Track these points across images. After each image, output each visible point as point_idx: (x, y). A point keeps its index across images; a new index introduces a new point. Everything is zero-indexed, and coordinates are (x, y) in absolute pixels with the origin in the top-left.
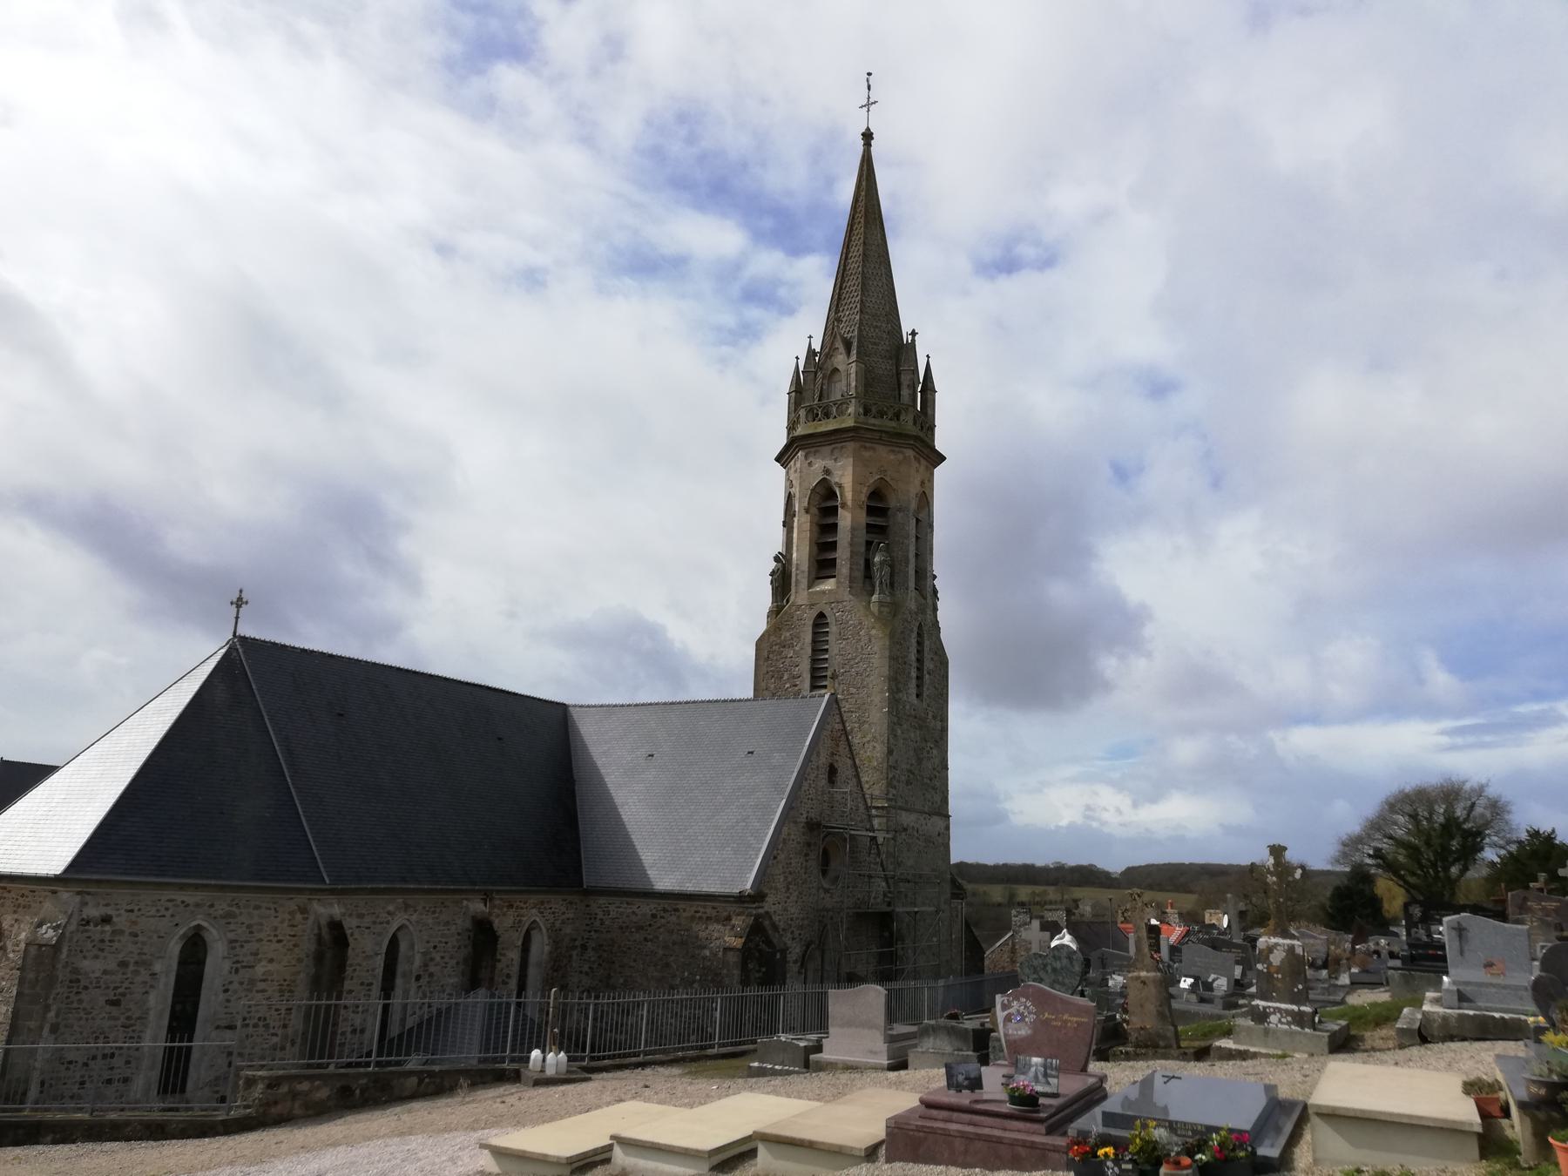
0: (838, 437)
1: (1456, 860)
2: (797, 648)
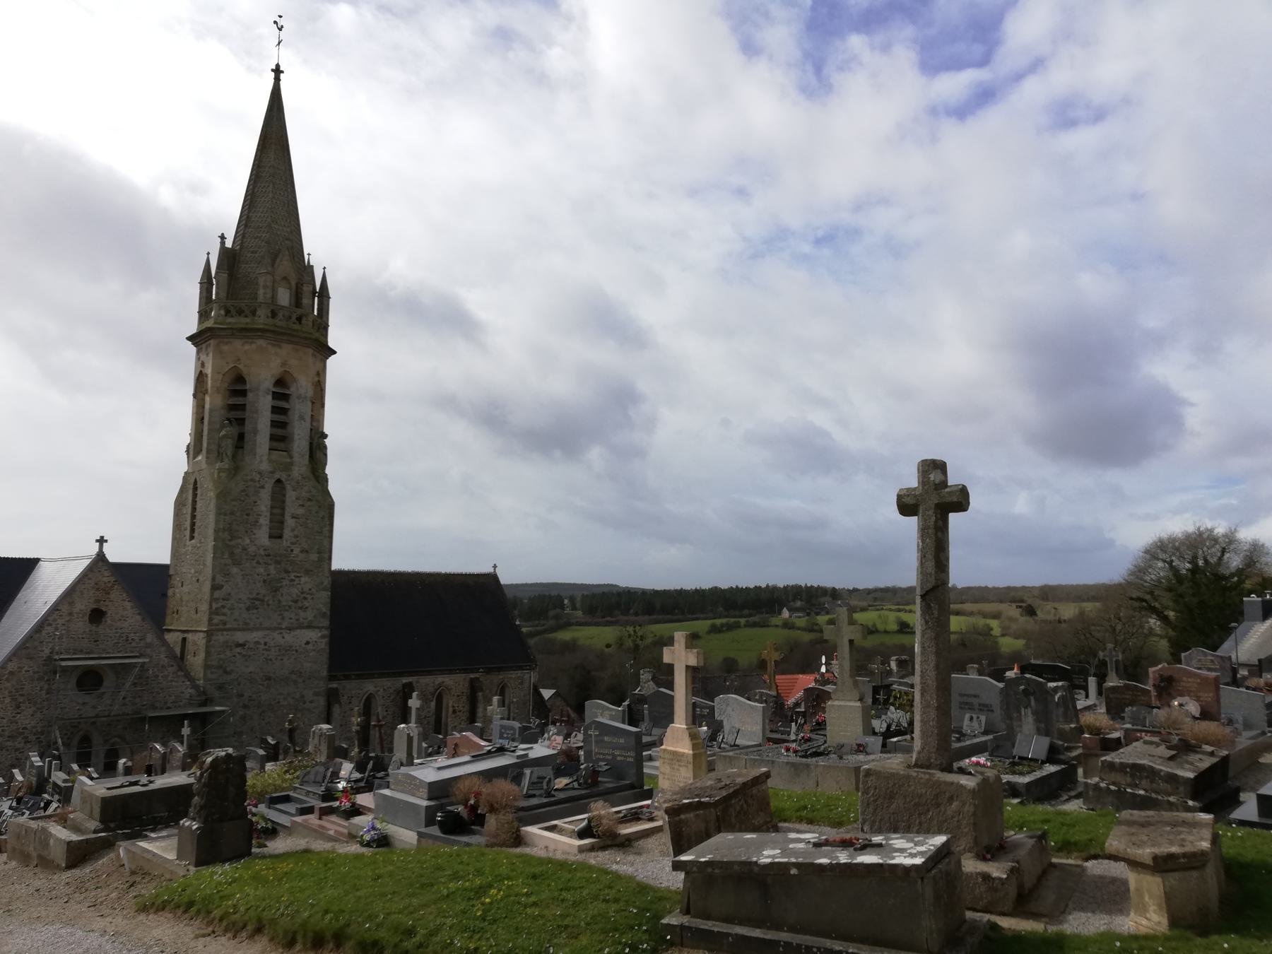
0: (205, 336)
1: (194, 682)
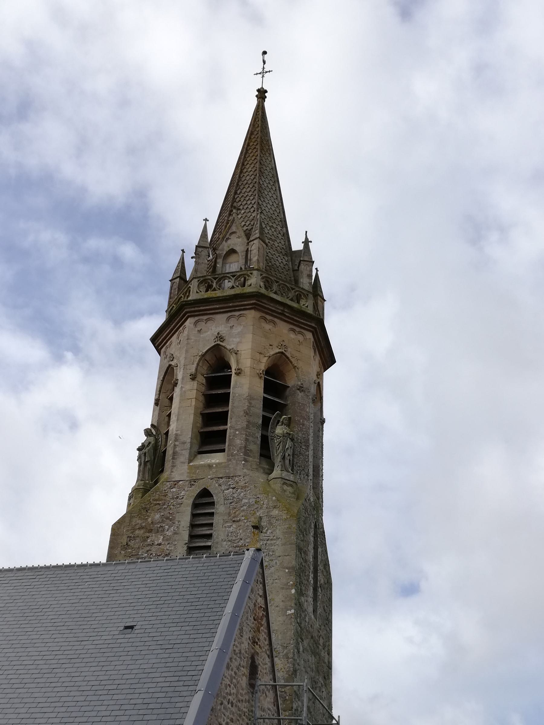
2: (169, 533)
